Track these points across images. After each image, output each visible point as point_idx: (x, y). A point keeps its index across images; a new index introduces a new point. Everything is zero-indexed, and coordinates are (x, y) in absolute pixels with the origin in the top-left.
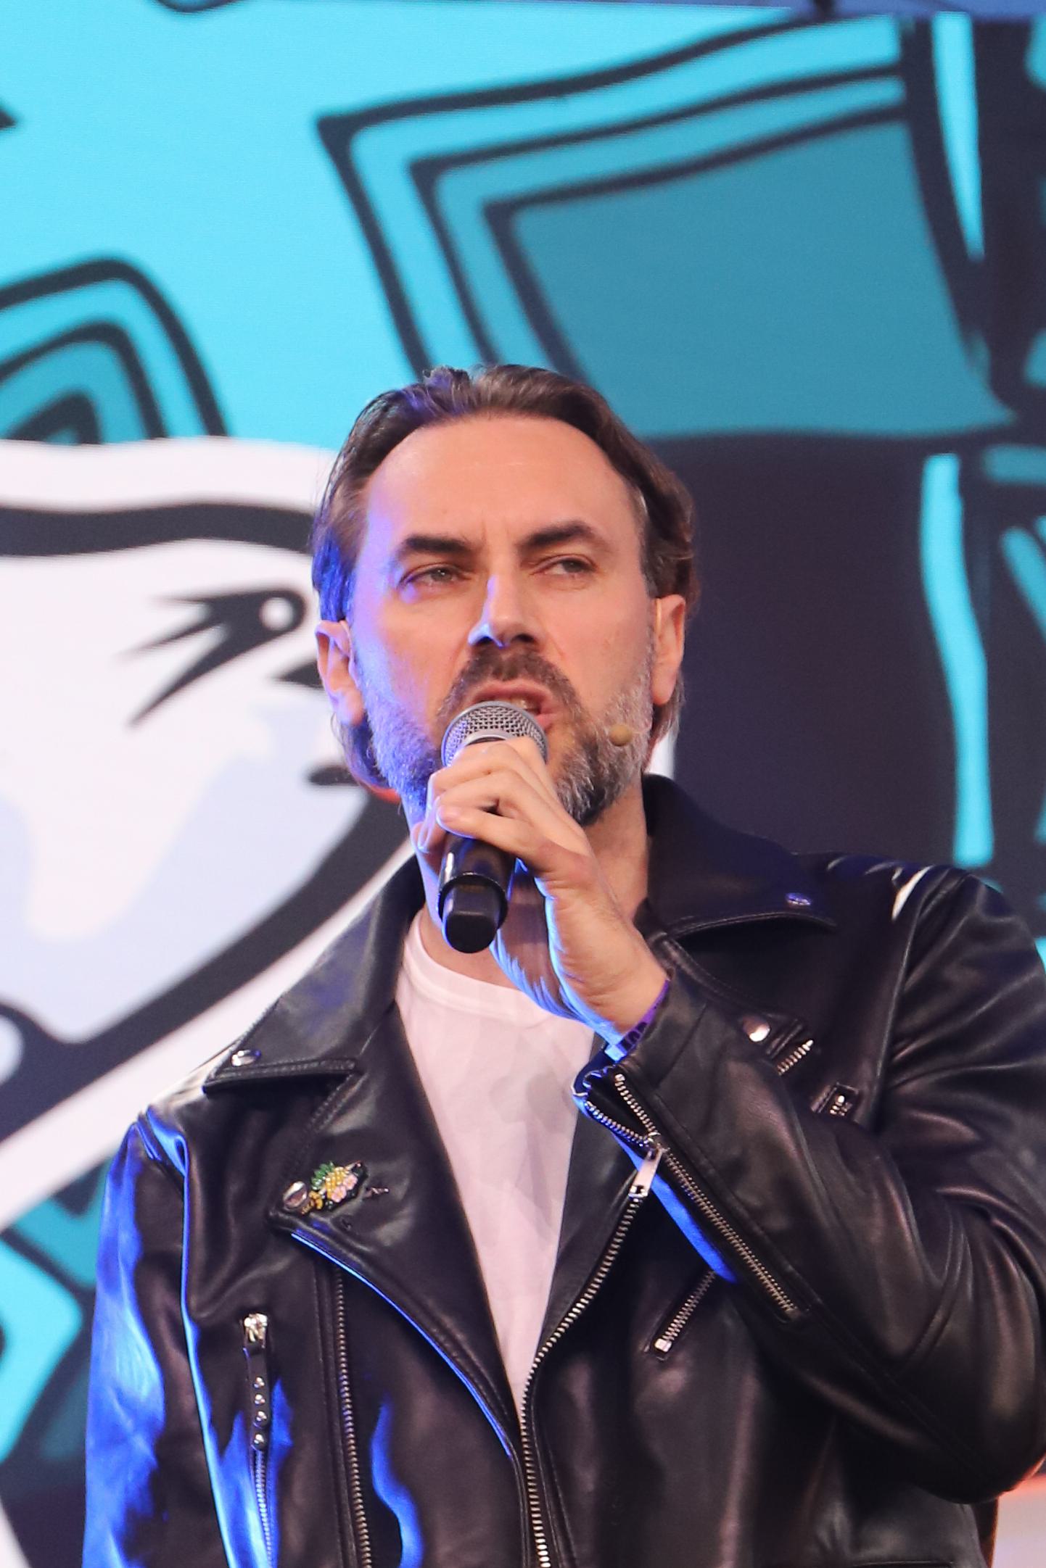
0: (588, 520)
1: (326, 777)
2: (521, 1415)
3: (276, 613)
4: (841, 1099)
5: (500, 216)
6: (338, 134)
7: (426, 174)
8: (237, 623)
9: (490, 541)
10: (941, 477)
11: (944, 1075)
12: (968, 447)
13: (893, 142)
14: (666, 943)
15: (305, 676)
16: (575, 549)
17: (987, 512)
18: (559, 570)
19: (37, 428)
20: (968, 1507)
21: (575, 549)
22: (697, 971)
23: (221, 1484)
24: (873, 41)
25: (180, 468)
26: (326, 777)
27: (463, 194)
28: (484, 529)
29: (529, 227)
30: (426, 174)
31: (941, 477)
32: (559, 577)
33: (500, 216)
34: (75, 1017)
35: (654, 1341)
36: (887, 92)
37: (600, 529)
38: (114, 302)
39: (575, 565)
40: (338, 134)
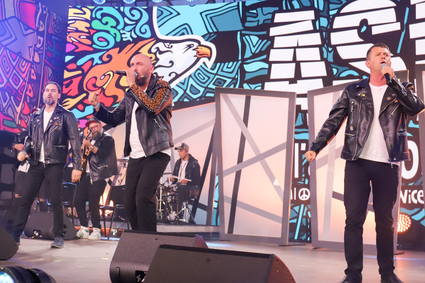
1: (195, 56)
3: (192, 46)
5: (211, 18)
6: (201, 13)
7: (206, 15)
8: (190, 46)
10: (239, 33)
12: (241, 31)
13: (237, 10)
15: (194, 50)
17: (242, 35)
19: (181, 35)
20: (147, 270)
24: (236, 4)
25: (190, 36)
26: (195, 56)
27: (209, 17)
29: (213, 18)
30: (206, 15)
31: (239, 33)
33: (211, 18)
34: (179, 73)
36: (236, 7)
40: (201, 13)
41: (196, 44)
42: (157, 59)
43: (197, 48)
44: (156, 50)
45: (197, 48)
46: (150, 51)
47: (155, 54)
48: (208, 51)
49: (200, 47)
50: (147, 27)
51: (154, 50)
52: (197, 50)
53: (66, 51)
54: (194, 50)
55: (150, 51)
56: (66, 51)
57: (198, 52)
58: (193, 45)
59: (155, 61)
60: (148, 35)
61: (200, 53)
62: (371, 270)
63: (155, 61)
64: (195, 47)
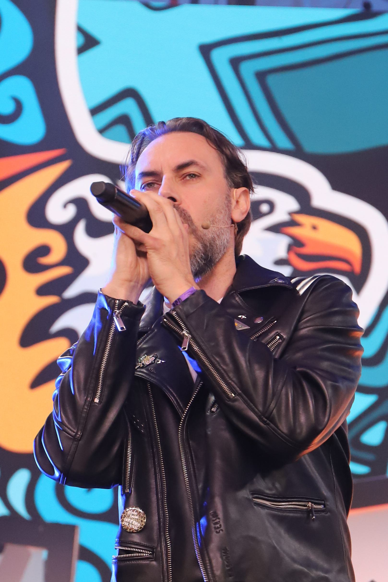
0: (197, 160)
2: (130, 442)
3: (265, 208)
4: (278, 337)
5: (261, 76)
6: (206, 50)
7: (235, 63)
9: (163, 170)
11: (316, 327)
14: (235, 294)
15: (276, 229)
16: (192, 169)
18: (188, 178)
21: (192, 169)
22: (242, 302)
23: (309, 391)
27: (248, 69)
28: (161, 166)
29: (271, 80)
30: (235, 63)
32: (188, 180)
33: (261, 76)
35: (211, 408)
37: (202, 163)
38: (128, 107)
39: (193, 176)
40: (206, 50)
41: (285, 204)
42: (77, 262)
43: (293, 223)
44: (72, 211)
45: (293, 223)
46: (36, 216)
47: (67, 230)
48: (351, 243)
49: (307, 220)
50: (23, 88)
51: (58, 211)
52: (295, 231)
53: (219, 302)
54: (276, 229)
55: (36, 216)
56: (219, 302)
57: (296, 244)
58: (272, 205)
59: (65, 270)
60: (30, 128)
61: (305, 250)
62: (166, 581)
63: (65, 270)
64: (280, 216)
